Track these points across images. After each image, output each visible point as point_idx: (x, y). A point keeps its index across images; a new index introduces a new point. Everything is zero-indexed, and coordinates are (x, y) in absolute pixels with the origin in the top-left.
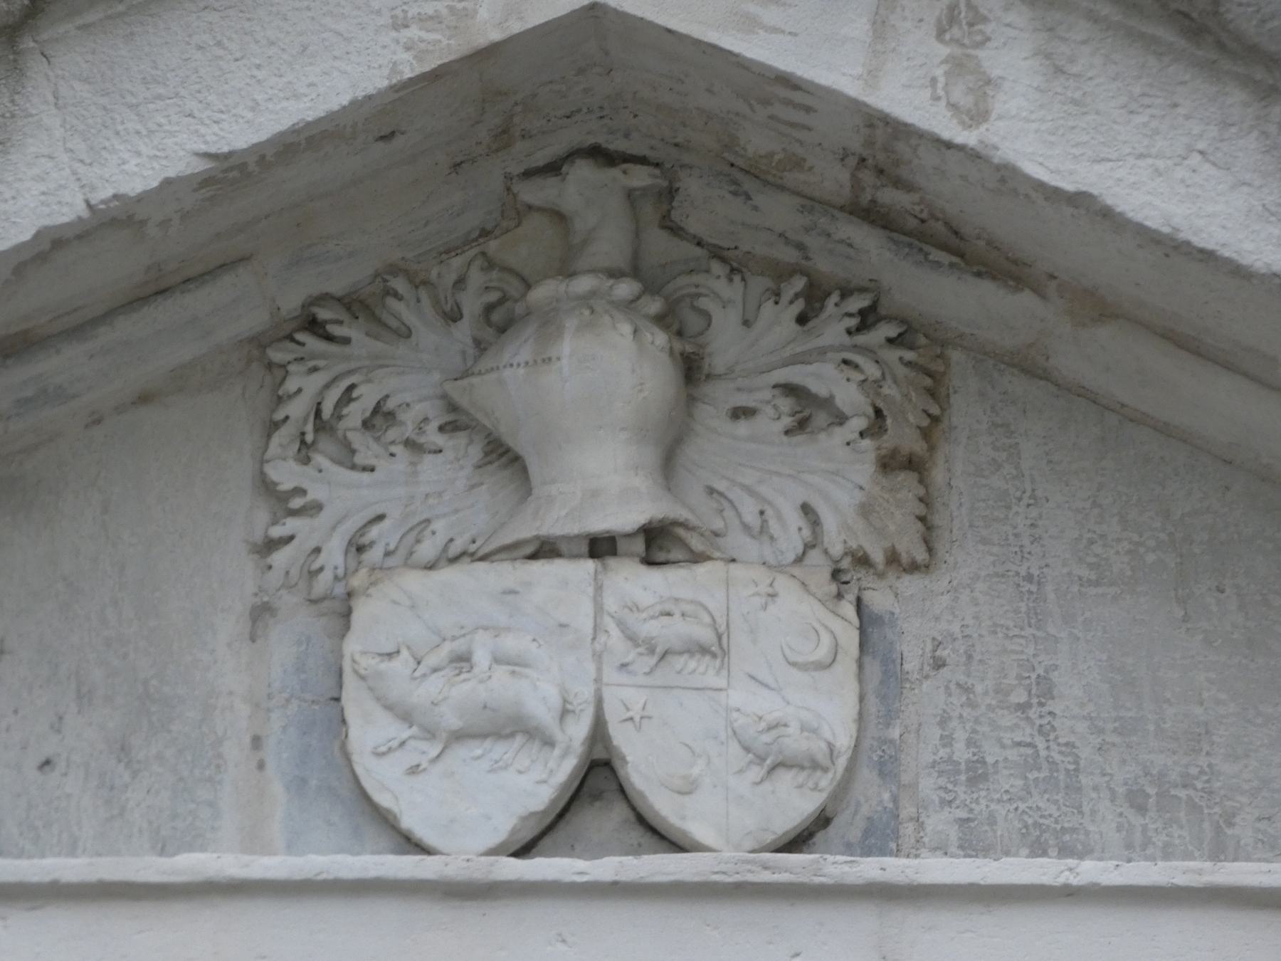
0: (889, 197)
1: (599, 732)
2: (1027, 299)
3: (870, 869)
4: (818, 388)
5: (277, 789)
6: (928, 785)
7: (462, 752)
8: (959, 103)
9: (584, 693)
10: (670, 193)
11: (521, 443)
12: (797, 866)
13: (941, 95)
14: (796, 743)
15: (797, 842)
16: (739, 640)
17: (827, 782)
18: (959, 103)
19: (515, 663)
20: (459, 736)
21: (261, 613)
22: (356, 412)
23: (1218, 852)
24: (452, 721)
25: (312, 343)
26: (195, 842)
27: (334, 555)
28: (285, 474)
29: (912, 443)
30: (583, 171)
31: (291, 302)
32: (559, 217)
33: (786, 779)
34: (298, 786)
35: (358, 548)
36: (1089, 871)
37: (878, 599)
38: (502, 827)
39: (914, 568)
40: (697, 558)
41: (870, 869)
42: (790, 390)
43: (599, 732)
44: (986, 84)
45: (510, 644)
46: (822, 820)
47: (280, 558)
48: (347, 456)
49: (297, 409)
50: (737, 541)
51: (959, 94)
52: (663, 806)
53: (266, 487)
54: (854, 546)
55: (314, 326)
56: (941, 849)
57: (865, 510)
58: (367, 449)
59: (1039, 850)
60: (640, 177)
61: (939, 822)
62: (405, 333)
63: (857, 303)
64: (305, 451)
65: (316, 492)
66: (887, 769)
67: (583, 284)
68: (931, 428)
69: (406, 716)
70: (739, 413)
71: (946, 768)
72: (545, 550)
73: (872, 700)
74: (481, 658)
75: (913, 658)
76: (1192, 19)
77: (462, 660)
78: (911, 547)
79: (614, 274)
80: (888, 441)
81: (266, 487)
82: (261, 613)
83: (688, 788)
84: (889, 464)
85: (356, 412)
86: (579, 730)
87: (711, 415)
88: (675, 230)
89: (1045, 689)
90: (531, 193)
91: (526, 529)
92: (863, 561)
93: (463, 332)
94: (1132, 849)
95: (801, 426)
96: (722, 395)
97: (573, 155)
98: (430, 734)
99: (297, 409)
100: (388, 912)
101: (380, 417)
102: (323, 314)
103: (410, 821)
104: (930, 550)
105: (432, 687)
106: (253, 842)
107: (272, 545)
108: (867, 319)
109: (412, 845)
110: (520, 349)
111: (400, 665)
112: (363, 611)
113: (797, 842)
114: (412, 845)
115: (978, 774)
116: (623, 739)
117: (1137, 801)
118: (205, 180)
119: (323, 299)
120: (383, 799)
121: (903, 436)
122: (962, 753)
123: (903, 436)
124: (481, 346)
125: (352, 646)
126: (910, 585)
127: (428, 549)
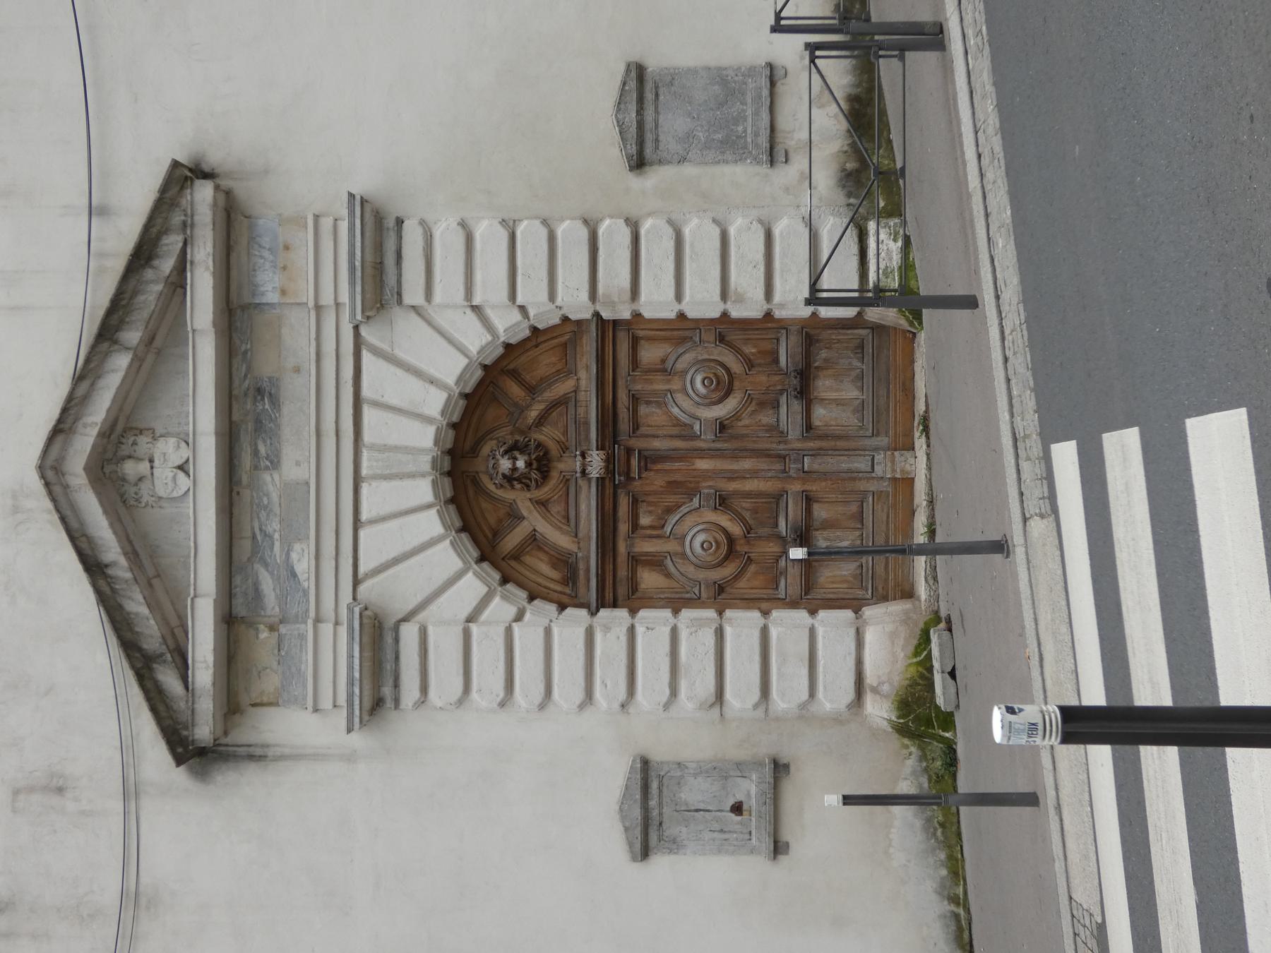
0: (108, 433)
1: (174, 468)
2: (121, 418)
3: (191, 436)
4: (131, 442)
5: (182, 505)
6: (181, 429)
7: (177, 483)
8: (257, 218)
9: (170, 470)
10: (107, 460)
11: (139, 476)
12: (191, 444)
13: (49, 471)
14: (176, 444)
15: (188, 444)
16: (164, 451)
17: (181, 441)
18: (257, 218)
19: (166, 478)
20: (175, 483)
21: (160, 507)
22: (135, 496)
23: (188, 396)
24: (173, 485)
25: (127, 502)
26: (188, 515)
27: (153, 499)
28: (143, 504)
29: (139, 431)
30: (105, 470)
31: (121, 504)
32: (110, 472)
33: (180, 446)
34: (182, 503)
35: (152, 496)
36: (191, 410)
37: (158, 435)
38: (187, 479)
39: (154, 431)
40: (153, 456)
41: (191, 436)
42: (132, 445)
43: (174, 468)
44: (92, 423)
45: (164, 477)
46: (185, 442)
47: (154, 505)
48: (141, 497)
49: (135, 503)
50: (151, 451)
51: (94, 425)
52: (184, 460)
53: (145, 507)
54: (910, 769)
55: (124, 502)
56: (189, 428)
57: (147, 436)
58: (140, 495)
59: (188, 416)
60: (105, 463)
61: (185, 428)
62: (126, 491)
63: (121, 438)
64: (140, 502)
65: (145, 500)
66: (179, 434)
67: (119, 470)
68: (136, 429)
69: (173, 490)
70: (135, 451)
71: (178, 427)
72: (152, 474)
73: (505, 534)
74: (165, 481)
75: (165, 431)
76: (286, 606)
77: (166, 484)
78: (151, 431)
79: (117, 466)
80: (138, 433)
81: (145, 507)
82: (160, 507)
83: (182, 457)
84: (141, 433)
85: (135, 496)
86: (174, 470)
87: (136, 455)
88: (111, 460)
89: (169, 415)
90: (107, 475)
91: (150, 476)
92: (153, 437)
93: (125, 484)
94: (188, 405)
95: (136, 444)
96: (133, 453)
97: (102, 472)
98: (175, 487)
99: (135, 503)
100: (197, 494)
101: (136, 494)
102: (123, 500)
103: (186, 489)
104: (151, 429)
105: (170, 487)
106: (189, 508)
107: (152, 507)
108: (123, 437)
109: (189, 490)
110: (127, 477)
111: (167, 491)
112: (160, 495)
113: (188, 444)
114: (189, 490)
115: (179, 424)
116: (175, 465)
117: (182, 405)
118: (106, 515)
119: (121, 500)
120: (183, 493)
121: (138, 432)
122: (177, 425)
123: (138, 432)
124: (127, 482)
125: (165, 496)
126: (156, 431)
127: (152, 488)
